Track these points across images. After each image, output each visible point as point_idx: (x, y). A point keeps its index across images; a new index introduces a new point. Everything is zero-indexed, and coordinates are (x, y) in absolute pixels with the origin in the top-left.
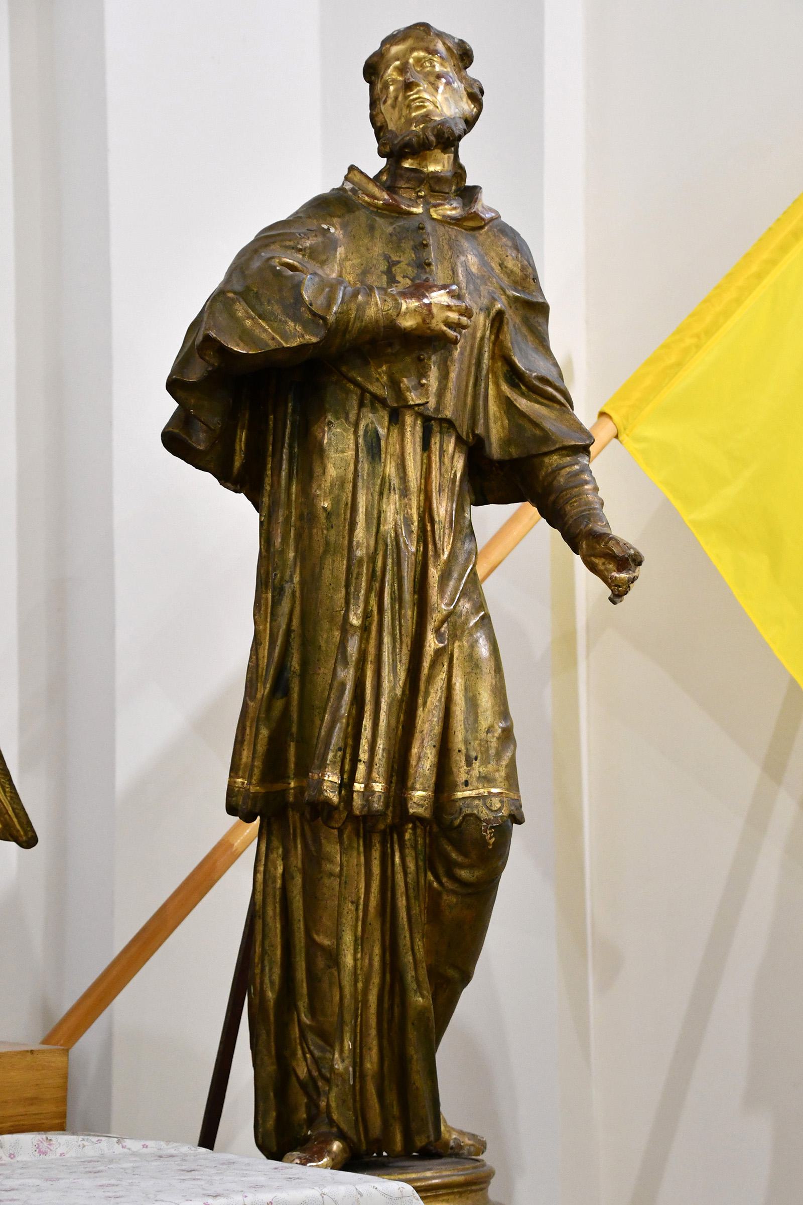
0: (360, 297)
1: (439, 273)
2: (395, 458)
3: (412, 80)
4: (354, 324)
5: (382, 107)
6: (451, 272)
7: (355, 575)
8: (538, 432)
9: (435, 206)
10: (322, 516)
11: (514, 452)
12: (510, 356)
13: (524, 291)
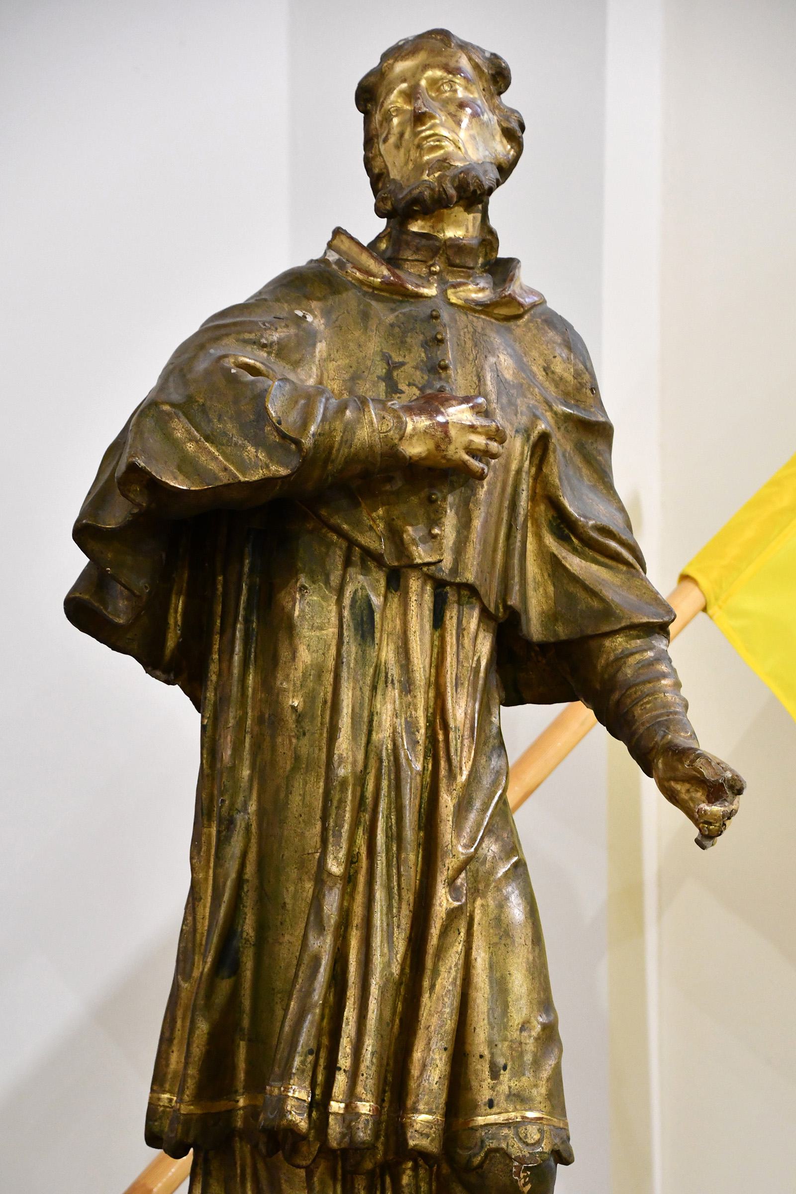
0: (348, 413)
1: (459, 379)
3: (424, 109)
4: (339, 450)
5: (382, 147)
6: (475, 379)
7: (335, 803)
8: (595, 604)
9: (455, 286)
10: (291, 719)
11: (562, 631)
12: (557, 497)
13: (578, 406)
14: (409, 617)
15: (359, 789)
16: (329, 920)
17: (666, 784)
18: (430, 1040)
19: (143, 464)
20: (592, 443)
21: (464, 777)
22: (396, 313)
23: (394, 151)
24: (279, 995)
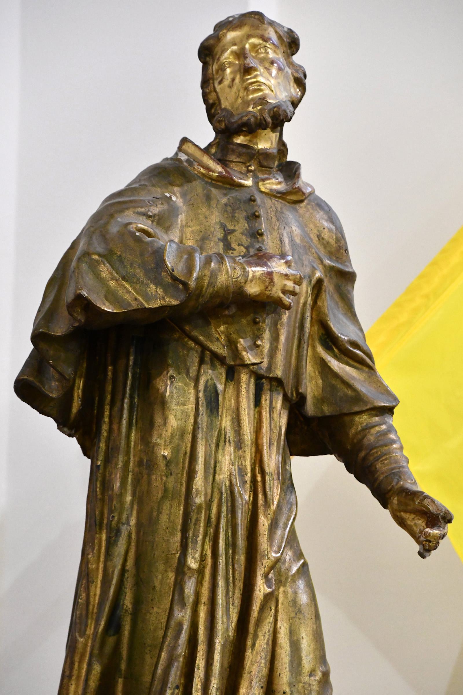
0: (212, 264)
1: (269, 243)
2: (231, 412)
3: (251, 65)
4: (207, 289)
5: (218, 88)
6: (279, 242)
7: (193, 521)
8: (350, 392)
9: (263, 180)
10: (162, 464)
11: (327, 410)
12: (327, 321)
13: (337, 261)
14: (241, 399)
15: (208, 512)
16: (189, 598)
17: (398, 514)
18: (252, 681)
19: (86, 295)
20: (345, 286)
21: (275, 506)
22: (228, 197)
23: (227, 90)
24: (149, 648)
